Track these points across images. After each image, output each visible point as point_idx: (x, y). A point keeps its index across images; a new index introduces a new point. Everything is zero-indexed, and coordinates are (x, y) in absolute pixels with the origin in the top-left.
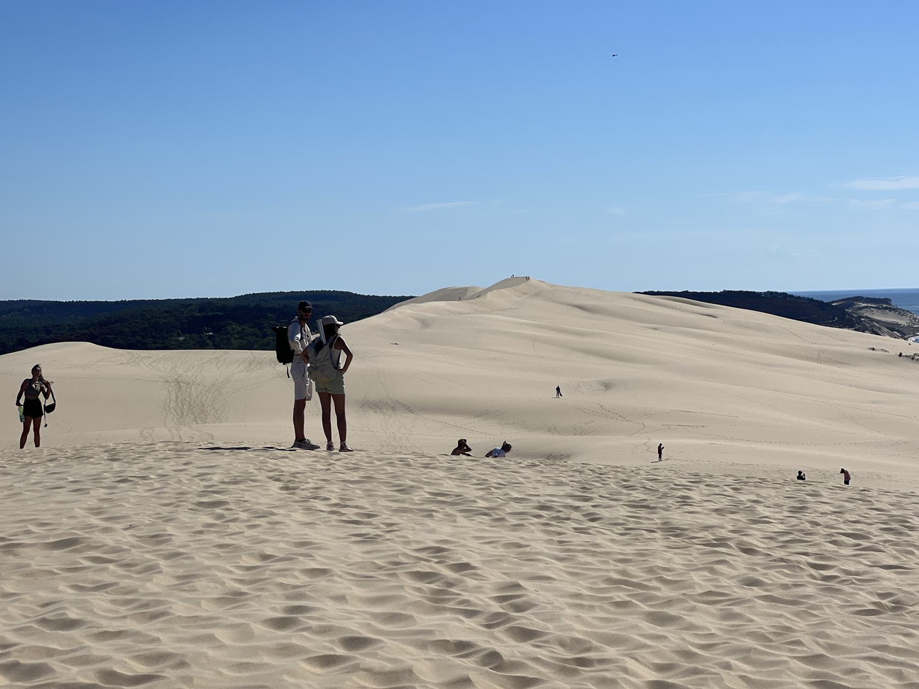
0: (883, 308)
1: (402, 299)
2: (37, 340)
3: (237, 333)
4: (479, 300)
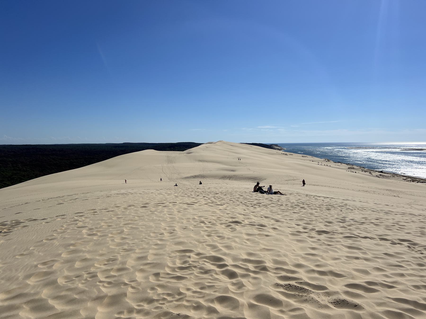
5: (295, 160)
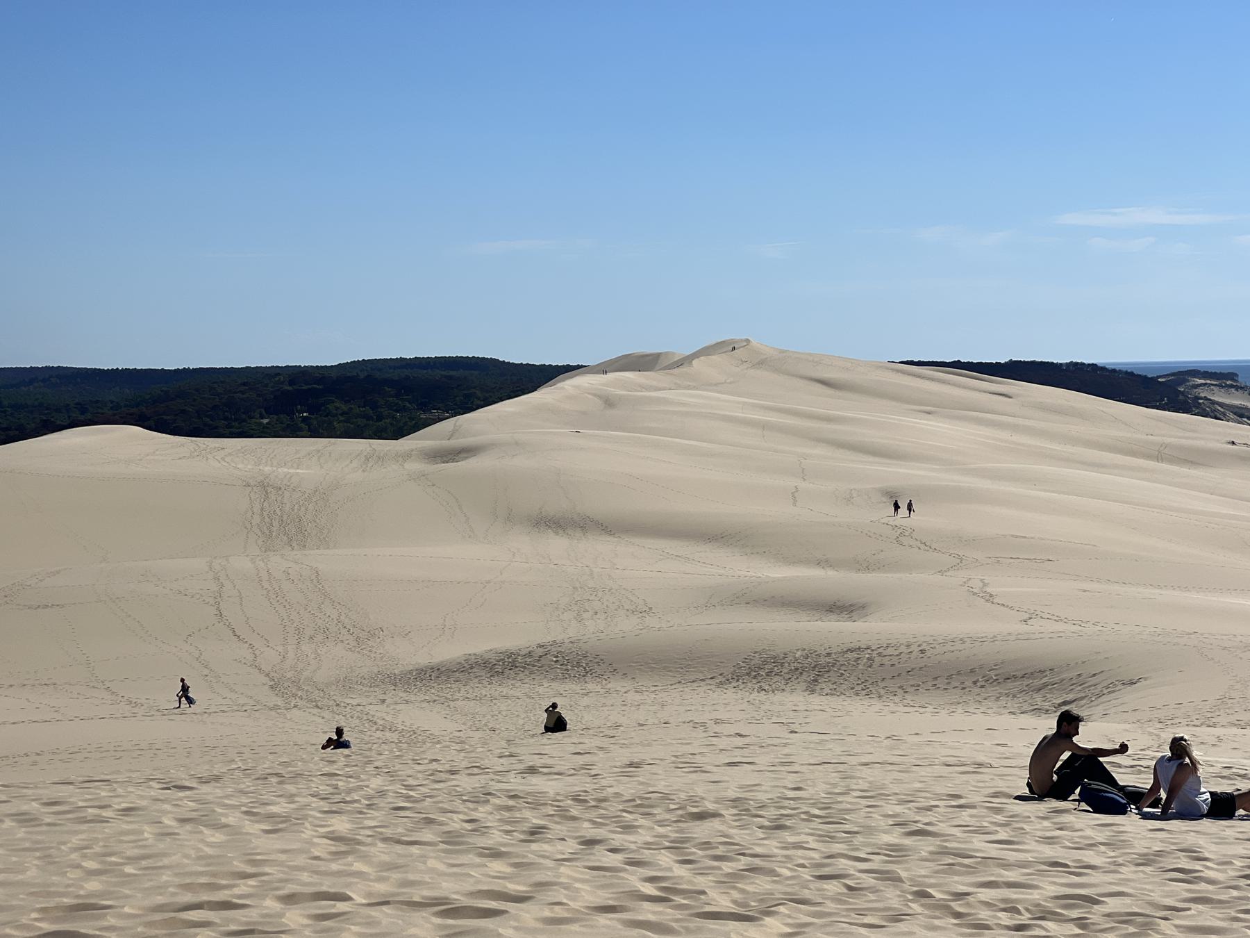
0: (1227, 386)
1: (568, 369)
2: (67, 422)
3: (342, 415)
4: (677, 371)
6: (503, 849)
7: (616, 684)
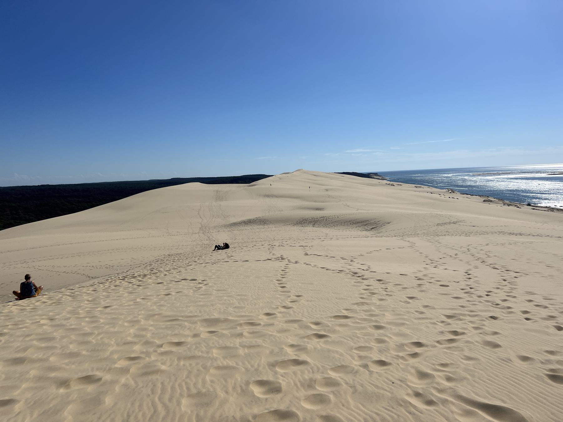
5: (408, 190)
6: (333, 319)
7: (270, 226)
